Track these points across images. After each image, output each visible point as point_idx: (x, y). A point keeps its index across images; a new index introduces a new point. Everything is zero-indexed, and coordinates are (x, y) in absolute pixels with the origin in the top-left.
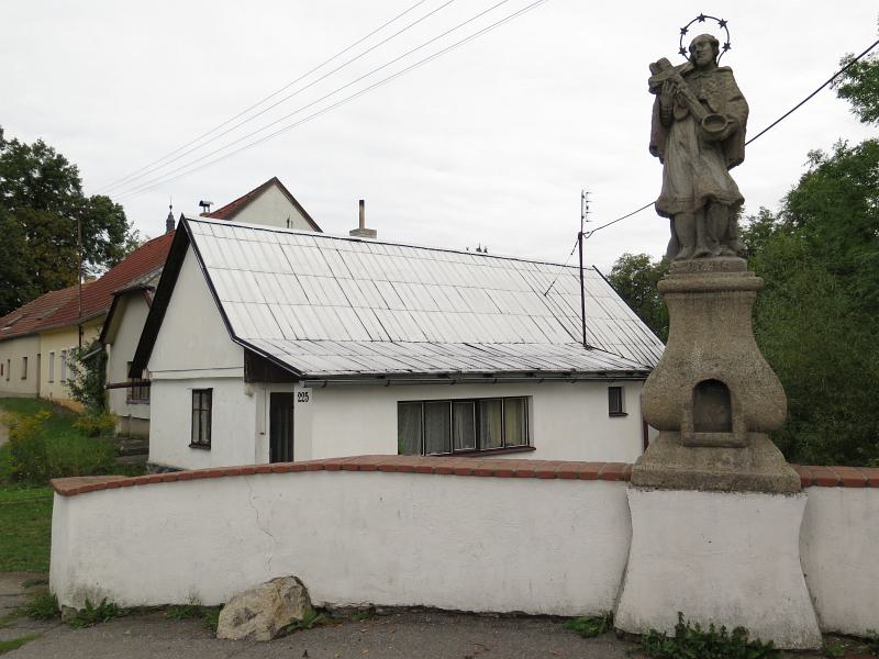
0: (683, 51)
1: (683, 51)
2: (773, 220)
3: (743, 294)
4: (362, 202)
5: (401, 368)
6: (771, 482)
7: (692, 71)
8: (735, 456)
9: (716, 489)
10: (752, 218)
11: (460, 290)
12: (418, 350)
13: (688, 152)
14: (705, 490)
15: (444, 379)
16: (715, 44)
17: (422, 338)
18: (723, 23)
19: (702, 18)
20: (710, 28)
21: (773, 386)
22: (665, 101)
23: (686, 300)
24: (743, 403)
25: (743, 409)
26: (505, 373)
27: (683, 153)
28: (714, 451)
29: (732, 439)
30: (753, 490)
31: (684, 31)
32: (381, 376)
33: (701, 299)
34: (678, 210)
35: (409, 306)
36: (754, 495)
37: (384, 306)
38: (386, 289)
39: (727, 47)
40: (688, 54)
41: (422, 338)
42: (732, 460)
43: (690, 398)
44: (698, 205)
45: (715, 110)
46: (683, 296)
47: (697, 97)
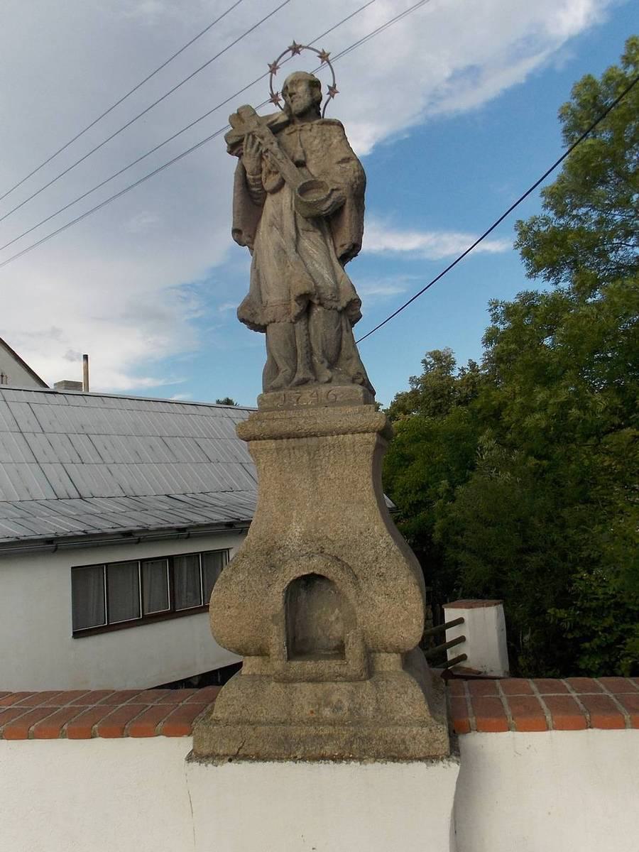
0: (274, 99)
1: (274, 99)
2: (479, 370)
3: (358, 437)
4: (86, 357)
5: (77, 528)
6: (404, 742)
7: (286, 124)
8: (352, 695)
9: (322, 758)
10: (462, 370)
11: (201, 442)
12: (109, 506)
13: (282, 234)
14: (303, 759)
15: (128, 538)
16: (315, 85)
17: (118, 492)
18: (324, 56)
19: (295, 49)
20: (307, 63)
21: (403, 581)
22: (250, 165)
23: (278, 450)
24: (359, 610)
25: (360, 620)
26: (199, 526)
27: (276, 233)
28: (319, 689)
29: (344, 670)
30: (377, 757)
31: (274, 68)
32: (49, 541)
33: (300, 448)
34: (270, 318)
35: (108, 460)
36: (377, 765)
37: (78, 460)
38: (82, 442)
39: (333, 91)
40: (282, 103)
41: (118, 492)
42: (346, 704)
43: (280, 606)
44: (296, 309)
45: (316, 176)
46: (272, 444)
47: (292, 160)
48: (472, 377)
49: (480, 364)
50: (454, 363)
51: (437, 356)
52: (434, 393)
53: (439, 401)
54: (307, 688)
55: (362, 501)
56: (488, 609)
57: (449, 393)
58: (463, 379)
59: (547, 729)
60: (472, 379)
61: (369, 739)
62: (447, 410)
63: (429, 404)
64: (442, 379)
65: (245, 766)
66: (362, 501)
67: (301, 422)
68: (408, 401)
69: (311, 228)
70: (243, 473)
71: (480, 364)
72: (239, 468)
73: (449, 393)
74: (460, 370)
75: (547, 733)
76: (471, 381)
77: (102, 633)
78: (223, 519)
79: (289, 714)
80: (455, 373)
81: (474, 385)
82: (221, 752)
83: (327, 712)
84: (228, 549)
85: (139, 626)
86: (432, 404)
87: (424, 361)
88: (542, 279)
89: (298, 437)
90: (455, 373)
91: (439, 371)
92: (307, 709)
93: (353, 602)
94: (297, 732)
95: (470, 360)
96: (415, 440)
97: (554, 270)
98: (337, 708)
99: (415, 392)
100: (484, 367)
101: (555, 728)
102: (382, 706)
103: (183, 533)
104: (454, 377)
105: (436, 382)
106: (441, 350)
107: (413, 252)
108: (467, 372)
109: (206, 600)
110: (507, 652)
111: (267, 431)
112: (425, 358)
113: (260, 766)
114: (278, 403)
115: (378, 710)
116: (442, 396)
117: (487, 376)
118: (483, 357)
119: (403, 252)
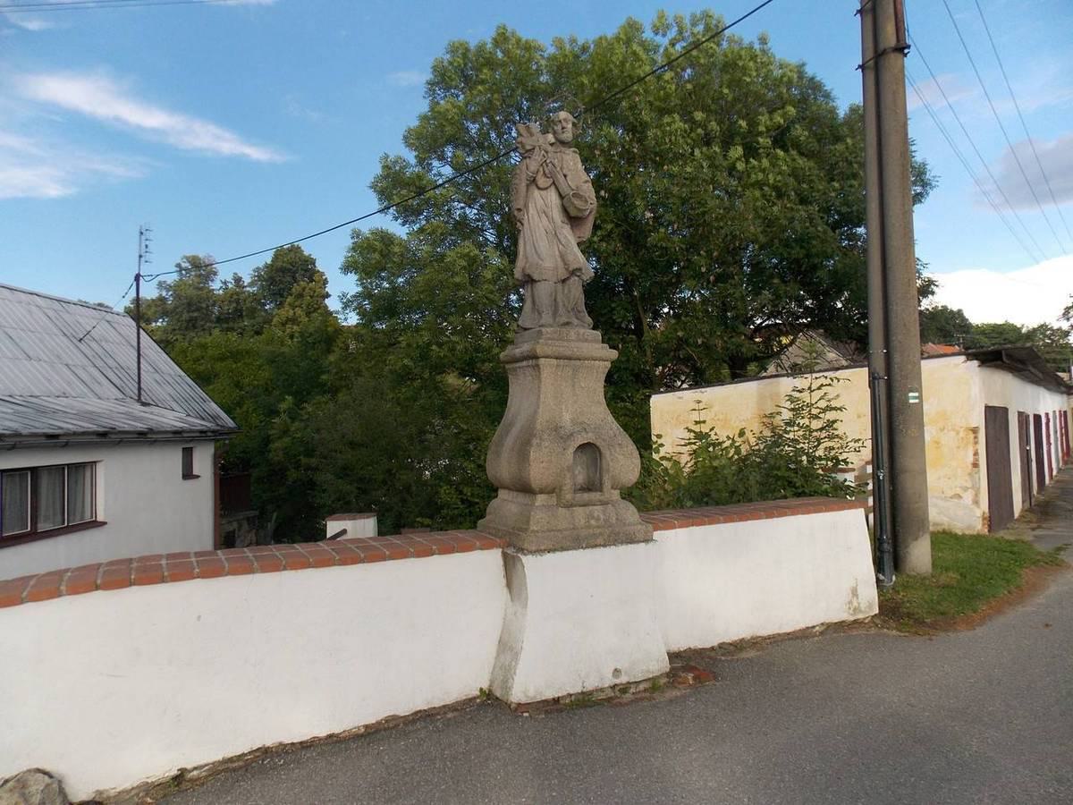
8: (604, 512)
9: (596, 546)
10: (225, 283)
24: (611, 464)
25: (611, 469)
30: (622, 543)
42: (602, 517)
46: (554, 362)
48: (237, 294)
49: (247, 280)
50: (215, 274)
51: (196, 264)
52: (189, 304)
53: (196, 314)
54: (580, 510)
55: (599, 402)
56: (367, 521)
57: (208, 306)
58: (226, 294)
59: (675, 528)
60: (236, 293)
61: (619, 533)
62: (202, 326)
63: (181, 316)
64: (201, 289)
65: (558, 554)
66: (599, 402)
67: (575, 350)
68: (153, 309)
69: (566, 221)
70: (69, 373)
71: (247, 280)
72: (65, 369)
73: (208, 306)
74: (222, 283)
75: (673, 531)
76: (235, 297)
77: (20, 544)
78: (94, 428)
79: (573, 524)
80: (216, 285)
81: (237, 302)
82: (543, 548)
83: (593, 522)
84: (95, 462)
85: (13, 545)
86: (185, 316)
87: (178, 265)
88: (391, 218)
89: (570, 358)
90: (216, 285)
91: (196, 280)
92: (583, 521)
93: (609, 459)
94: (584, 533)
95: (235, 274)
96: (222, 358)
97: (407, 213)
98: (598, 519)
99: (162, 299)
100: (251, 285)
101: (679, 527)
102: (620, 518)
103: (54, 440)
104: (213, 290)
105: (191, 292)
106: (201, 255)
107: (154, 131)
108: (230, 286)
109: (71, 518)
110: (322, 569)
111: (556, 354)
112: (179, 261)
113: (565, 553)
114: (556, 336)
115: (617, 519)
116: (198, 310)
117: (255, 295)
118: (252, 272)
119: (139, 128)
